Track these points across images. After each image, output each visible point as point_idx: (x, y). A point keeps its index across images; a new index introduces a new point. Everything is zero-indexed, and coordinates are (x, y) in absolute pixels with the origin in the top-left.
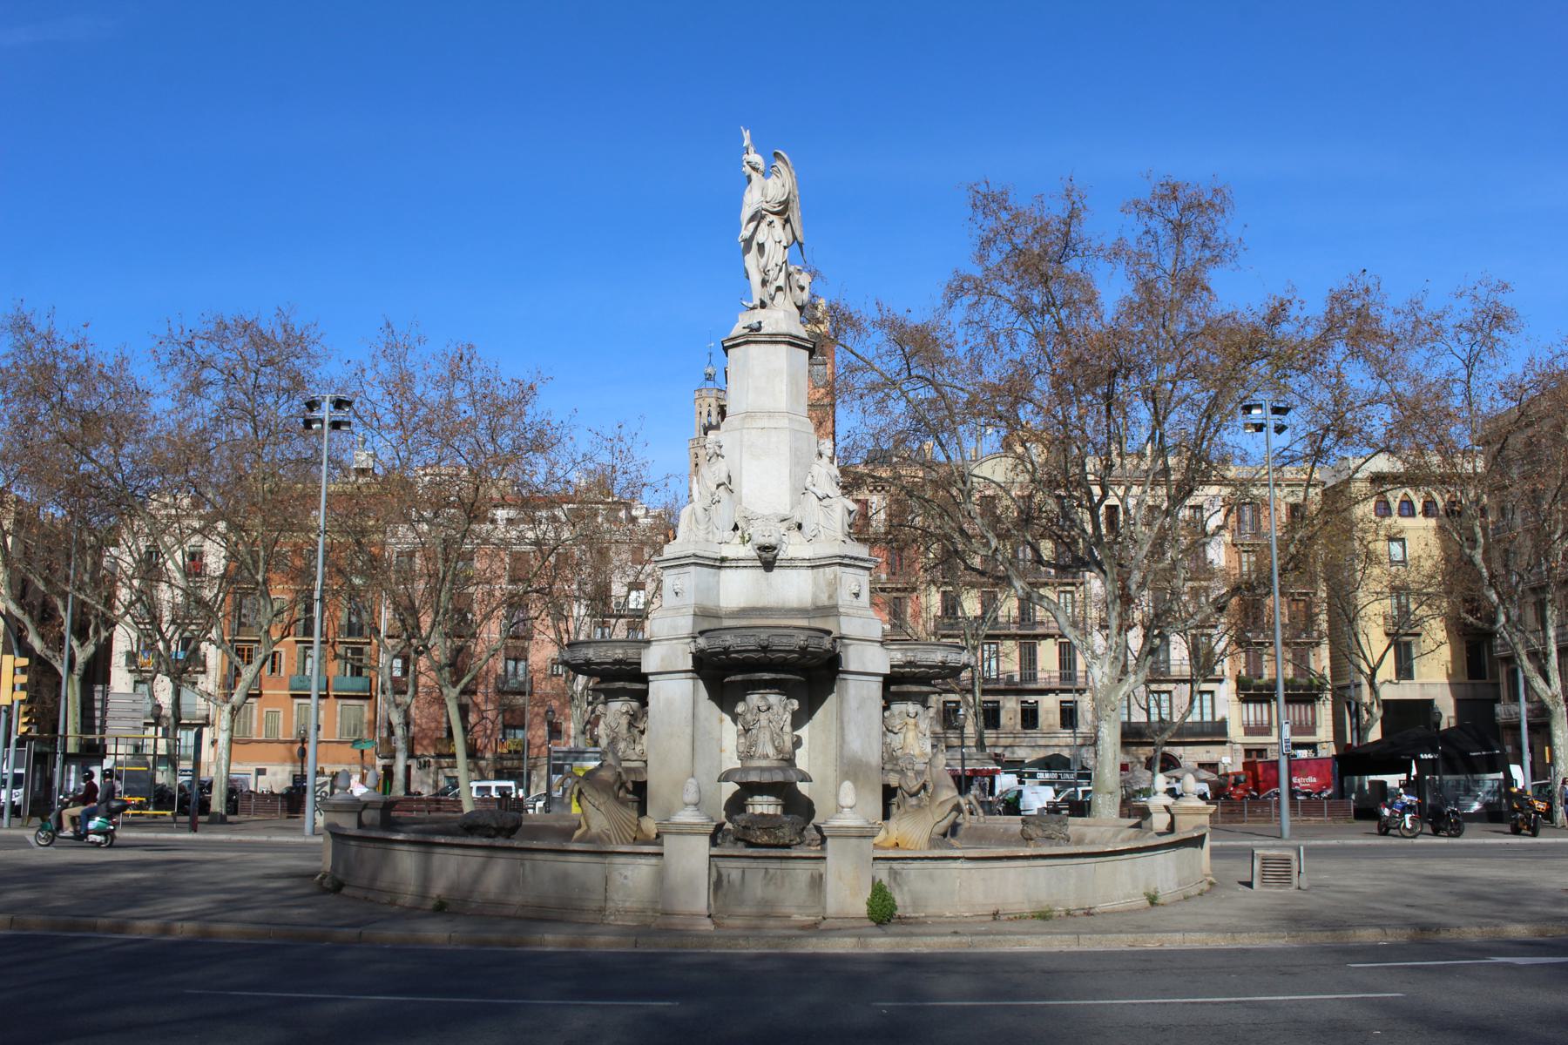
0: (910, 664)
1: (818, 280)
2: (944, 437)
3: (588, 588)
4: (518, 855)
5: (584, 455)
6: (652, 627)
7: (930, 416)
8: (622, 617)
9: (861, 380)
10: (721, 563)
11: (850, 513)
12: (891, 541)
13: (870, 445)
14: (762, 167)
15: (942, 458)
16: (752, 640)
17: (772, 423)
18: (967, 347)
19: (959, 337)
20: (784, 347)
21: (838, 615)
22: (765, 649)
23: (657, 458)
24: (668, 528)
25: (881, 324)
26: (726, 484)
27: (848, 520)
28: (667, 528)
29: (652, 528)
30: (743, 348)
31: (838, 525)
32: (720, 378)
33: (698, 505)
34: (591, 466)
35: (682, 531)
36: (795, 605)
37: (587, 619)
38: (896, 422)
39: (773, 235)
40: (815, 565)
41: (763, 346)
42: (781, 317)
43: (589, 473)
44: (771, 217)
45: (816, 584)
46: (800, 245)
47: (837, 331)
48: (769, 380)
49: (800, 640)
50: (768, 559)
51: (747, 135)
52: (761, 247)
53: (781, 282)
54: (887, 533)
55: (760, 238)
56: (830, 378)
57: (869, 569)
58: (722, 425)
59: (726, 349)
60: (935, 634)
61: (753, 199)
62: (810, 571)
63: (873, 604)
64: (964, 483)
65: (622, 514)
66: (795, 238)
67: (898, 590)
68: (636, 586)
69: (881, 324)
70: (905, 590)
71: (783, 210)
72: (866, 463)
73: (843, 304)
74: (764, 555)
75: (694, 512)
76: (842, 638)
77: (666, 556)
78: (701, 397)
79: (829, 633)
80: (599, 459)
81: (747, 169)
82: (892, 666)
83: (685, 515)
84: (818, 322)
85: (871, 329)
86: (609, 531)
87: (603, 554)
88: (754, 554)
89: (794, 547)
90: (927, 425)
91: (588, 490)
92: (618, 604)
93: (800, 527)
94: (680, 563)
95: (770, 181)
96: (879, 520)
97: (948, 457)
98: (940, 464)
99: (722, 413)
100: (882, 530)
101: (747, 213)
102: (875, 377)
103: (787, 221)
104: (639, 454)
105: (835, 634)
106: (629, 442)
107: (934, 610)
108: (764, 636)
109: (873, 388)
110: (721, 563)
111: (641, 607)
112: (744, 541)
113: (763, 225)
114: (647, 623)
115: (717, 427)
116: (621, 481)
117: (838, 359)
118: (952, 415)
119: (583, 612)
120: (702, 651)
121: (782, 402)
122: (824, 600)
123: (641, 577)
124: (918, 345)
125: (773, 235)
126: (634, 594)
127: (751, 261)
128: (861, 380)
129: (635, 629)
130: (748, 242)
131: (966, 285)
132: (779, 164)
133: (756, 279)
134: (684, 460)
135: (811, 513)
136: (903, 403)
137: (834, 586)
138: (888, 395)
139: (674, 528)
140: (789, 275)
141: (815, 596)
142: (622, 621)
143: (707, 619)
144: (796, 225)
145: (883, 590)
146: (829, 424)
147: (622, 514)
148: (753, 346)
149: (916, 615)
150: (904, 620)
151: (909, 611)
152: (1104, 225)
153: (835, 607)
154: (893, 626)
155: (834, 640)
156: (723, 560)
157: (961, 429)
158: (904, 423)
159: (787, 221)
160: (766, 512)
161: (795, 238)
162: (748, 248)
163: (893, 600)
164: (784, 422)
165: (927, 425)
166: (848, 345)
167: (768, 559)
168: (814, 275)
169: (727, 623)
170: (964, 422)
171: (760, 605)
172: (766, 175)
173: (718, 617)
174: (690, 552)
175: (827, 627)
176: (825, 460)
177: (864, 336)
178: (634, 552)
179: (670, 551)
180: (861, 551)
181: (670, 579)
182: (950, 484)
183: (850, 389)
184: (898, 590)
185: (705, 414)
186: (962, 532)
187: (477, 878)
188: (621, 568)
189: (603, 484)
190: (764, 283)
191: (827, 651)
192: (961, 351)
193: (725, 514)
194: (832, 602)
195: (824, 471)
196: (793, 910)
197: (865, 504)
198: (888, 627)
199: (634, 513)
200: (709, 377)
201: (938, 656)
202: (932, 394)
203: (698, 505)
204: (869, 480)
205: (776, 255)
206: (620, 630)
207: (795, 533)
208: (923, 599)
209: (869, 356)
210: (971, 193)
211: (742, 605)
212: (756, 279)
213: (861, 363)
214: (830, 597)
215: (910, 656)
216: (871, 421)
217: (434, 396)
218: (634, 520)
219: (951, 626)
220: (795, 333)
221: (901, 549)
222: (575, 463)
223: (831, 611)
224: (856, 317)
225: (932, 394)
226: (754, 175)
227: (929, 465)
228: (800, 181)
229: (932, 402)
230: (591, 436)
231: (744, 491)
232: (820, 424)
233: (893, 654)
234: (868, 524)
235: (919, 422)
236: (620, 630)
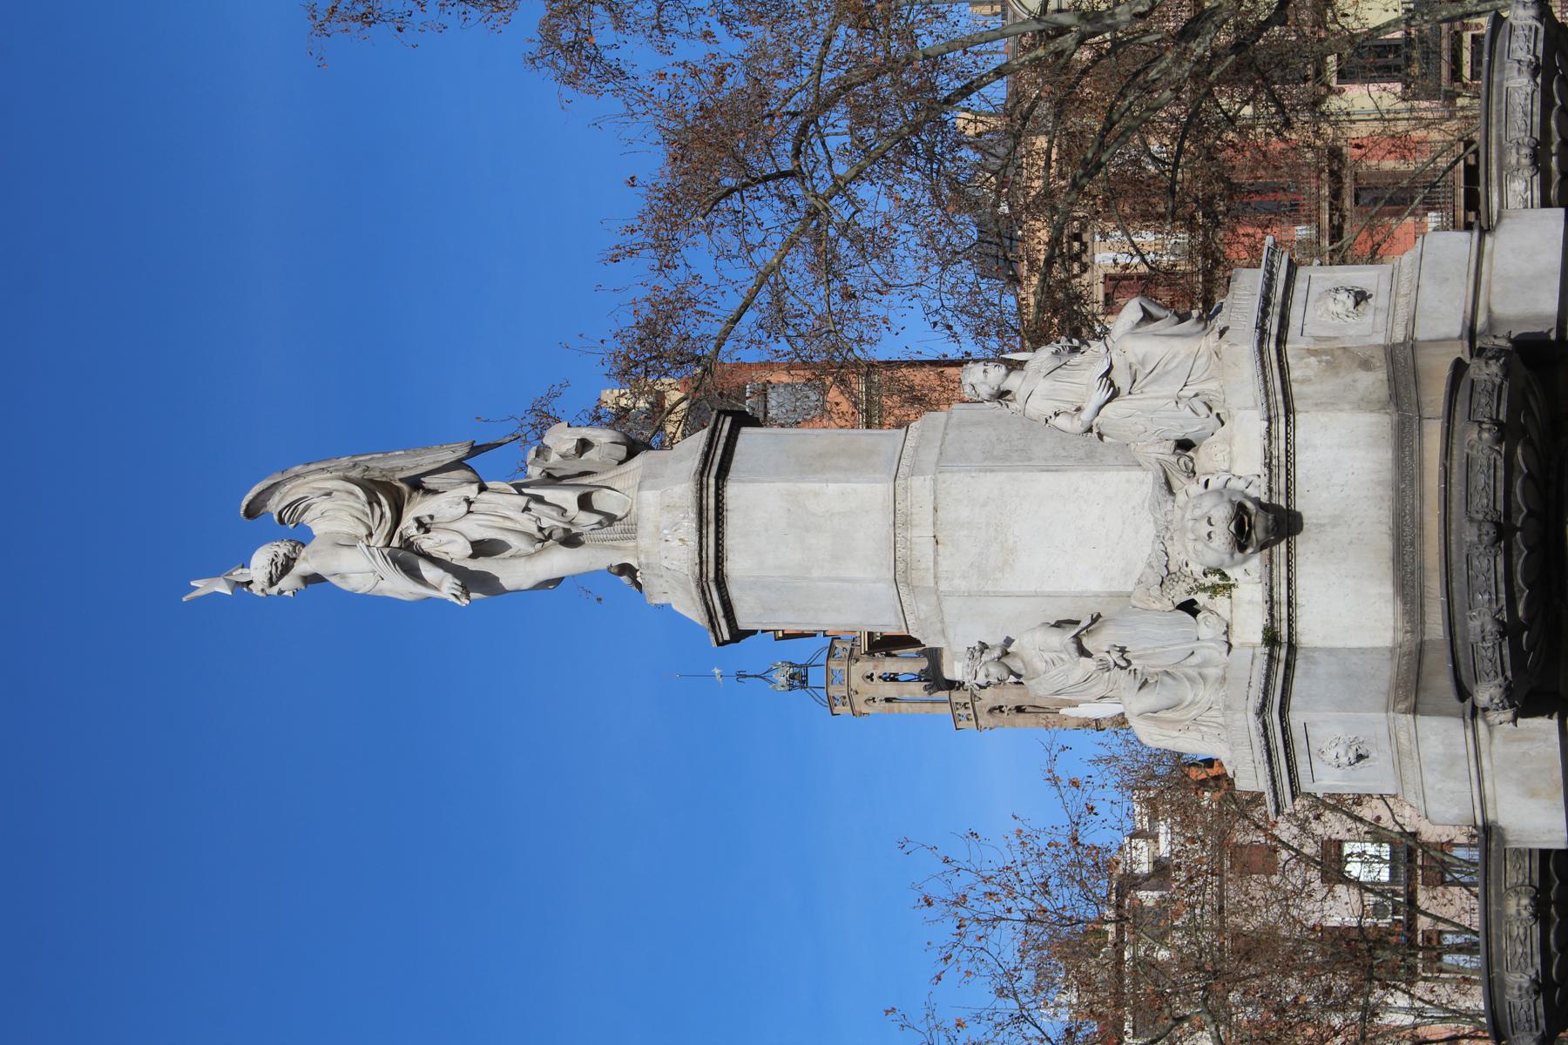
0: (1538, 158)
1: (556, 406)
2: (946, 84)
3: (1341, 985)
5: (1000, 992)
6: (1441, 815)
7: (896, 119)
8: (1411, 900)
9: (808, 295)
10: (1280, 644)
11: (1148, 317)
12: (1211, 215)
13: (966, 272)
14: (283, 549)
15: (998, 91)
16: (1481, 564)
17: (923, 516)
18: (720, 31)
19: (696, 52)
20: (732, 490)
21: (1412, 344)
22: (1503, 532)
23: (1005, 804)
24: (1183, 783)
25: (666, 249)
26: (1079, 630)
27: (1166, 324)
28: (1184, 784)
29: (1187, 823)
30: (734, 592)
31: (1182, 348)
32: (800, 652)
33: (1134, 704)
34: (1028, 976)
35: (1194, 745)
36: (1385, 455)
37: (1420, 989)
38: (911, 208)
39: (453, 518)
40: (1282, 405)
41: (730, 542)
42: (654, 502)
43: (1044, 982)
44: (408, 525)
46: (475, 450)
47: (683, 359)
48: (816, 527)
49: (1478, 441)
50: (1267, 525)
51: (203, 587)
52: (482, 548)
53: (567, 498)
54: (1191, 225)
55: (458, 551)
56: (800, 376)
57: (1292, 267)
58: (929, 643)
59: (738, 635)
60: (1451, 97)
61: (362, 570)
62: (1300, 418)
63: (1374, 257)
64: (1062, 30)
65: (1148, 897)
66: (458, 464)
67: (1336, 195)
68: (1331, 864)
69: (666, 249)
70: (1336, 177)
71: (389, 494)
72: (1016, 280)
73: (614, 345)
74: (1258, 534)
75: (1151, 714)
76: (1471, 333)
77: (1263, 785)
78: (848, 700)
79: (1459, 367)
80: (1010, 957)
81: (288, 584)
82: (1546, 203)
83: (1153, 736)
84: (658, 408)
85: (680, 274)
86: (1192, 929)
87: (1252, 947)
88: (1256, 563)
89: (1237, 456)
90: (916, 129)
91: (1086, 983)
92: (1378, 910)
93: (1185, 445)
94: (1281, 747)
95: (318, 528)
96: (1159, 245)
97: (999, 73)
98: (1017, 95)
99: (885, 645)
100: (1183, 237)
101: (398, 586)
102: (798, 260)
103: (416, 484)
104: (998, 853)
105: (1461, 350)
106: (967, 878)
107: (1388, 102)
108: (1471, 534)
109: (827, 267)
110: (1280, 644)
111: (1385, 850)
112: (1224, 587)
113: (427, 543)
114: (1430, 834)
115: (934, 656)
116: (1065, 897)
117: (751, 356)
118: (891, 65)
119: (1402, 1000)
120: (1509, 693)
121: (871, 492)
122: (1373, 381)
123: (1310, 849)
124: (717, 157)
125: (453, 518)
126: (1354, 869)
127: (515, 573)
128: (808, 295)
129: (1445, 867)
130: (470, 581)
131: (567, 36)
132: (275, 505)
133: (560, 562)
134: (1006, 750)
135: (1149, 415)
136: (864, 191)
137: (1336, 357)
138: (844, 230)
139: (1180, 762)
140: (551, 479)
142: (1423, 899)
143: (1423, 679)
144: (428, 460)
145: (1336, 233)
146: (917, 377)
147: (1148, 897)
148: (733, 568)
149: (1402, 145)
150: (1414, 177)
151: (1389, 164)
153: (1391, 352)
154: (1430, 205)
155: (1477, 352)
156: (1271, 639)
157: (926, 42)
158: (913, 186)
159: (416, 484)
160: (1149, 530)
161: (458, 464)
162: (486, 583)
163: (1363, 208)
164: (920, 486)
165: (916, 129)
166: (717, 329)
167: (1267, 525)
168: (545, 419)
169: (1436, 627)
170: (910, 37)
171: (1387, 544)
172: (302, 538)
173: (1418, 654)
174: (1253, 722)
175: (1445, 371)
176: (1014, 382)
177: (694, 291)
178: (1246, 870)
179: (1250, 776)
180: (1246, 288)
181: (1325, 775)
182: (1066, 68)
183: (830, 327)
184: (1336, 195)
185: (890, 689)
186: (1188, 33)
188: (1286, 899)
189: (1070, 946)
190: (571, 540)
191: (1507, 371)
192: (730, 46)
193: (1155, 636)
194: (1379, 360)
195: (1043, 385)
197: (1118, 284)
198: (1432, 219)
199: (1145, 868)
200: (799, 679)
201: (1519, 85)
202: (839, 118)
203: (1134, 704)
204: (1058, 272)
205: (501, 512)
206: (1452, 906)
207: (1203, 458)
208: (1361, 131)
209: (745, 276)
210: (334, 26)
211: (1388, 589)
212: (560, 562)
213: (764, 297)
214: (1366, 365)
215: (1519, 157)
216: (909, 270)
218: (1161, 869)
219: (1431, 55)
220: (694, 463)
221: (1233, 189)
222: (1022, 1018)
223: (1401, 364)
224: (646, 310)
225: (839, 118)
226: (303, 567)
227: (1018, 120)
228: (315, 454)
229: (860, 118)
230: (952, 975)
231: (1095, 585)
232: (920, 401)
233: (1513, 201)
234: (1170, 272)
235: (909, 150)
236: (1452, 906)
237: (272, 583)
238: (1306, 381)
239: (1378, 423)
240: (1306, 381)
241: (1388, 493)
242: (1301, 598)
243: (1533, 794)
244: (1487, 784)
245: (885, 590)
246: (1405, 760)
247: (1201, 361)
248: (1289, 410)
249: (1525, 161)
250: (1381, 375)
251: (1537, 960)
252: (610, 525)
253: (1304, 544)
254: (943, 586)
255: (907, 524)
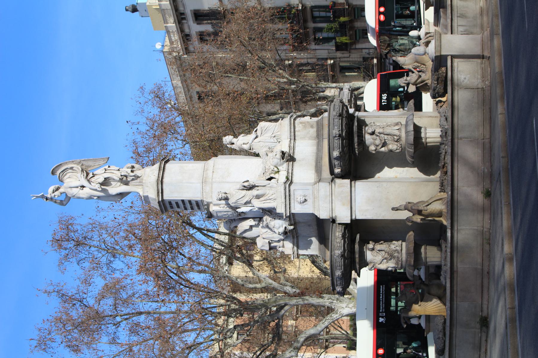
4: (456, 141)
10: (289, 181)
16: (336, 120)
45: (303, 138)
141: (310, 139)
148: (164, 180)
152: (71, 278)
156: (287, 179)
167: (289, 158)
187: (472, 168)
196: (478, 7)
211: (314, 172)
214: (312, 127)
217: (186, 250)
226: (61, 190)
237: (53, 192)
238: (299, 131)
239: (314, 142)
240: (299, 131)
241: (315, 154)
242: (294, 173)
243: (344, 205)
244: (333, 204)
245: (199, 186)
246: (316, 200)
247: (277, 127)
248: (294, 139)
249: (340, 236)
250: (315, 129)
251: (342, 248)
252: (137, 179)
253: (295, 164)
254: (213, 180)
255: (207, 170)
